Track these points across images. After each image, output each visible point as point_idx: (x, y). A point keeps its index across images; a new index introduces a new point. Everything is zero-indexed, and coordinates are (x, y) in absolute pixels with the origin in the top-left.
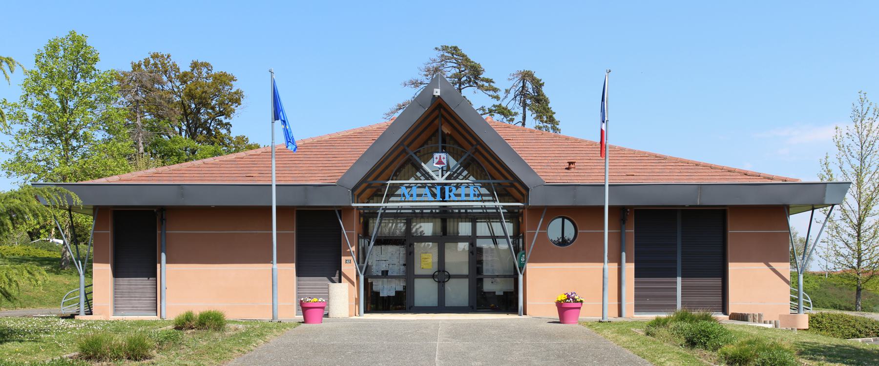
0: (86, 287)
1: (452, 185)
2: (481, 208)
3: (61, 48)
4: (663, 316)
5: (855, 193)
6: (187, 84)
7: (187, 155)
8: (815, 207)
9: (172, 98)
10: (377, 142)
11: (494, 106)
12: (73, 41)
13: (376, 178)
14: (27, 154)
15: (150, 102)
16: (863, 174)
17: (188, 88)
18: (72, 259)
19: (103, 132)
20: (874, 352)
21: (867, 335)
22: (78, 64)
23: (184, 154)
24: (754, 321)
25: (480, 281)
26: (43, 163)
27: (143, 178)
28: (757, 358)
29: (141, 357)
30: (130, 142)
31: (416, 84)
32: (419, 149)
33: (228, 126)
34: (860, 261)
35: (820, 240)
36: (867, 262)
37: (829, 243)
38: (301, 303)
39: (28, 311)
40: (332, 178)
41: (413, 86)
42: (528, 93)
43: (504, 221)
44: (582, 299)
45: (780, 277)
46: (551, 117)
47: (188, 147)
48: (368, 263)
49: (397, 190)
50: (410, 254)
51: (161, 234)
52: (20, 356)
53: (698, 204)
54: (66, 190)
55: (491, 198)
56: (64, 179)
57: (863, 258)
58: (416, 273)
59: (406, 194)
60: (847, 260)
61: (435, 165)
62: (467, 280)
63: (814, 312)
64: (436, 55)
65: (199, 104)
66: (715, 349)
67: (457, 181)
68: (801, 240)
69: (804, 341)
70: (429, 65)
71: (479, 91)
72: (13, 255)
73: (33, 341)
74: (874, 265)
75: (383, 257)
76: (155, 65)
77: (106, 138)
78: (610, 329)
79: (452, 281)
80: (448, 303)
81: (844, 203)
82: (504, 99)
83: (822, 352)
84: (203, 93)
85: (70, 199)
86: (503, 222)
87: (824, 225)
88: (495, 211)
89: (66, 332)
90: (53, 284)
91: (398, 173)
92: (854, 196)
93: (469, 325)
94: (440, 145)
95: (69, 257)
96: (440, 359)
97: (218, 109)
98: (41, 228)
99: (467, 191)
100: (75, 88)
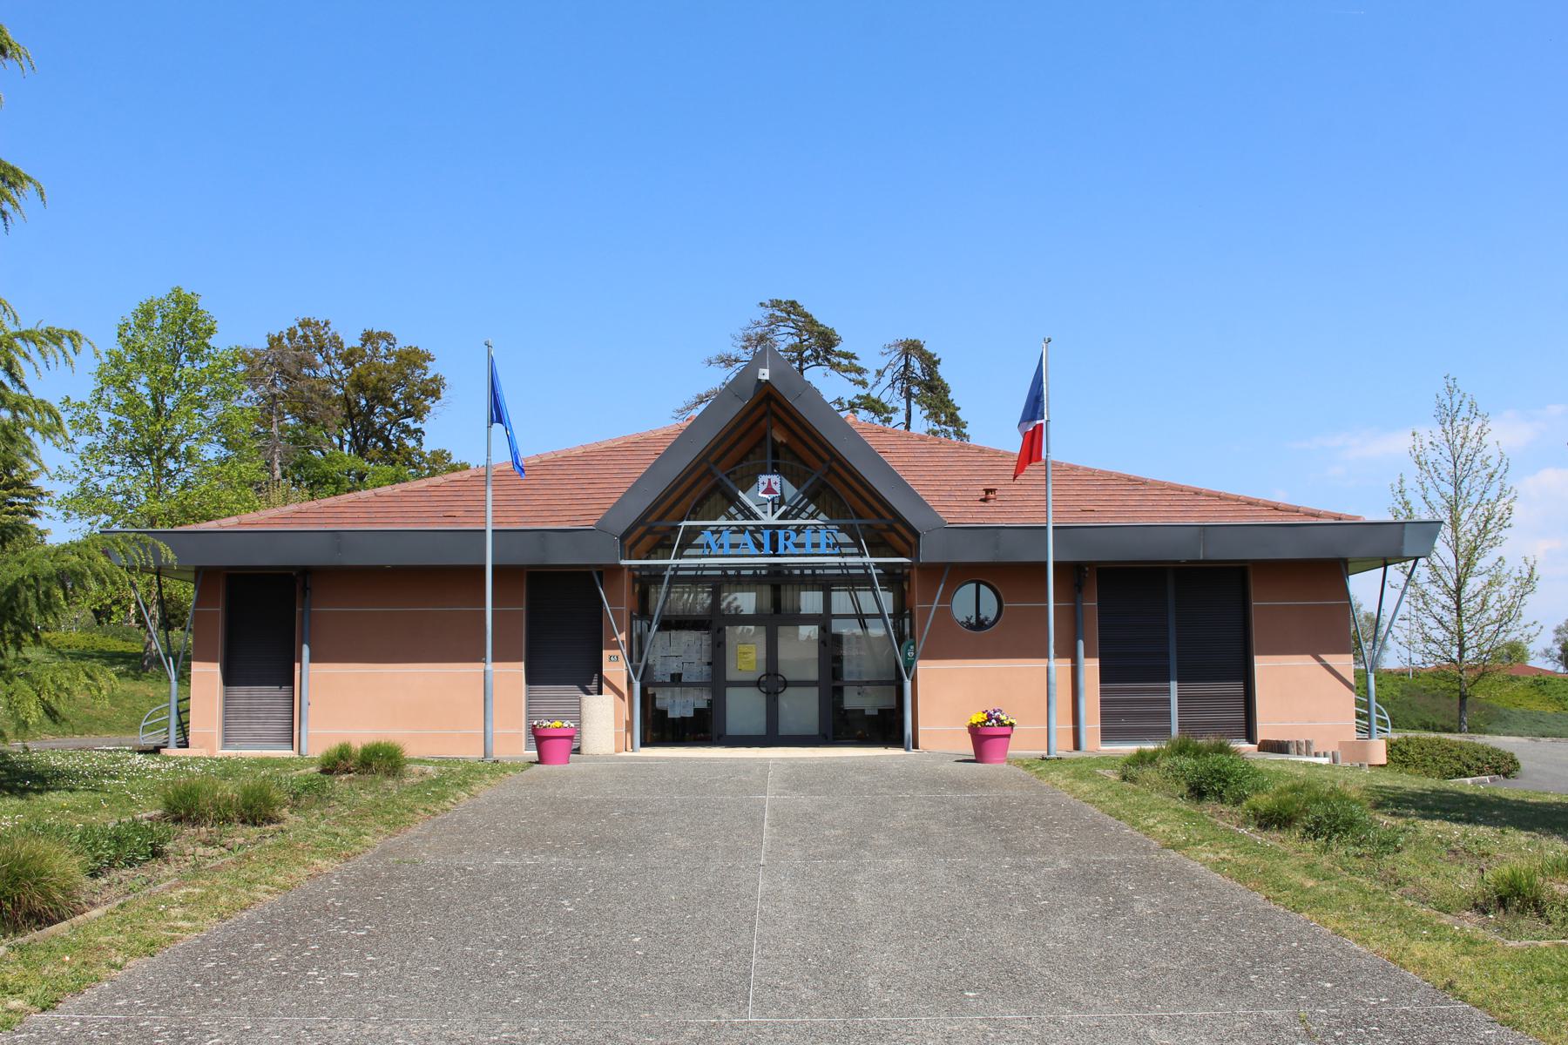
0: (179, 701)
1: (790, 528)
2: (840, 567)
3: (158, 314)
4: (1150, 747)
5: (1449, 539)
6: (354, 367)
7: (351, 483)
8: (1389, 561)
9: (329, 389)
10: (664, 457)
11: (858, 397)
12: (178, 303)
13: (660, 519)
14: (98, 483)
15: (294, 398)
16: (1460, 508)
17: (355, 375)
18: (159, 654)
19: (218, 447)
20: (1493, 800)
21: (1480, 772)
22: (182, 339)
23: (346, 482)
24: (1298, 754)
25: (838, 691)
26: (120, 498)
27: (277, 521)
28: (1307, 815)
29: (263, 820)
30: (260, 463)
31: (727, 361)
32: (733, 469)
33: (419, 434)
34: (1462, 650)
35: (1398, 617)
36: (1473, 651)
37: (1412, 622)
38: (534, 730)
39: (89, 740)
40: (586, 517)
41: (722, 365)
42: (914, 375)
43: (879, 588)
44: (1013, 721)
45: (1345, 680)
46: (953, 414)
47: (352, 469)
48: (647, 661)
49: (697, 537)
50: (718, 646)
51: (302, 614)
52: (69, 815)
53: (1201, 558)
54: (151, 539)
55: (855, 550)
56: (153, 524)
57: (1467, 645)
58: (728, 678)
59: (712, 544)
60: (1442, 649)
61: (760, 494)
62: (815, 690)
63: (1395, 736)
64: (761, 315)
65: (373, 399)
66: (1237, 802)
67: (798, 522)
68: (1367, 617)
69: (1381, 784)
70: (749, 331)
71: (834, 373)
72: (69, 647)
73: (90, 790)
74: (1485, 655)
75: (673, 651)
76: (305, 338)
77: (222, 455)
78: (1061, 771)
79: (790, 691)
80: (783, 730)
81: (1433, 555)
82: (874, 386)
83: (1411, 802)
84: (379, 381)
85: (157, 553)
86: (876, 590)
87: (1403, 592)
88: (862, 571)
89: (144, 776)
90: (130, 696)
91: (698, 509)
92: (1448, 544)
93: (821, 766)
94: (769, 461)
95: (156, 651)
96: (772, 825)
97: (402, 407)
98: (114, 603)
99: (816, 538)
100: (177, 375)
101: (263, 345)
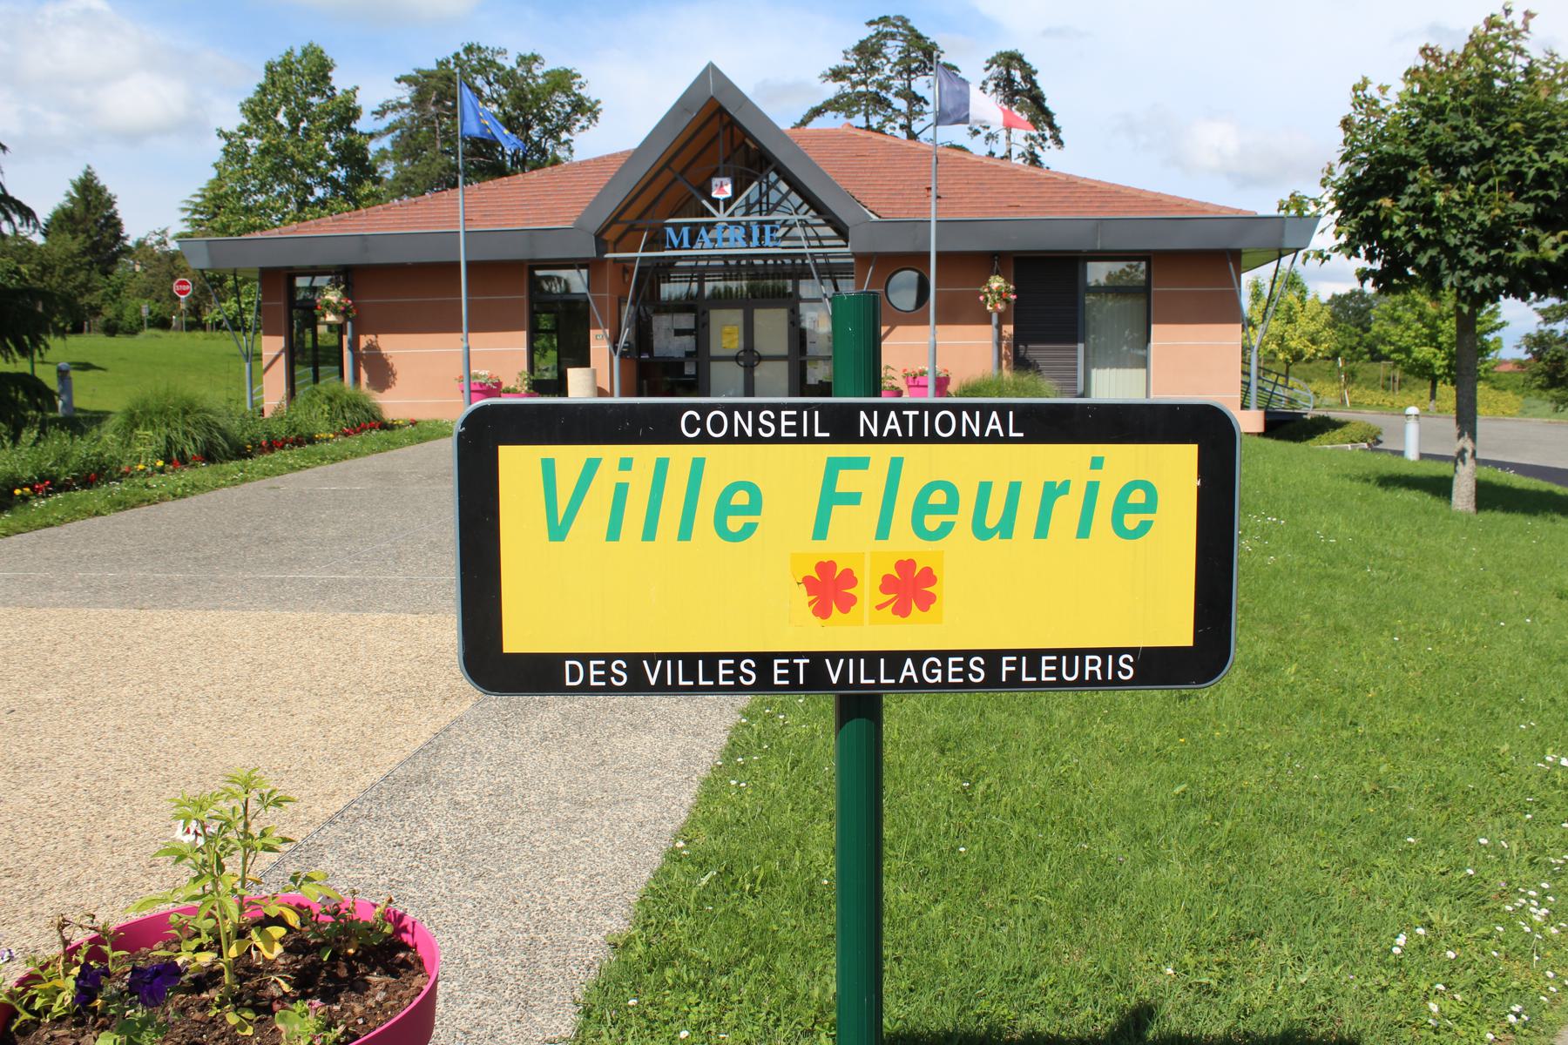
79: (763, 364)
101: (434, 67)
